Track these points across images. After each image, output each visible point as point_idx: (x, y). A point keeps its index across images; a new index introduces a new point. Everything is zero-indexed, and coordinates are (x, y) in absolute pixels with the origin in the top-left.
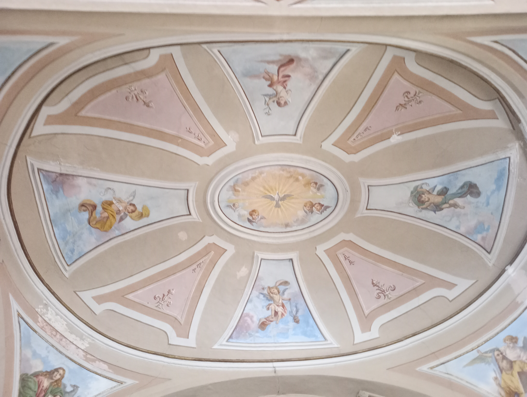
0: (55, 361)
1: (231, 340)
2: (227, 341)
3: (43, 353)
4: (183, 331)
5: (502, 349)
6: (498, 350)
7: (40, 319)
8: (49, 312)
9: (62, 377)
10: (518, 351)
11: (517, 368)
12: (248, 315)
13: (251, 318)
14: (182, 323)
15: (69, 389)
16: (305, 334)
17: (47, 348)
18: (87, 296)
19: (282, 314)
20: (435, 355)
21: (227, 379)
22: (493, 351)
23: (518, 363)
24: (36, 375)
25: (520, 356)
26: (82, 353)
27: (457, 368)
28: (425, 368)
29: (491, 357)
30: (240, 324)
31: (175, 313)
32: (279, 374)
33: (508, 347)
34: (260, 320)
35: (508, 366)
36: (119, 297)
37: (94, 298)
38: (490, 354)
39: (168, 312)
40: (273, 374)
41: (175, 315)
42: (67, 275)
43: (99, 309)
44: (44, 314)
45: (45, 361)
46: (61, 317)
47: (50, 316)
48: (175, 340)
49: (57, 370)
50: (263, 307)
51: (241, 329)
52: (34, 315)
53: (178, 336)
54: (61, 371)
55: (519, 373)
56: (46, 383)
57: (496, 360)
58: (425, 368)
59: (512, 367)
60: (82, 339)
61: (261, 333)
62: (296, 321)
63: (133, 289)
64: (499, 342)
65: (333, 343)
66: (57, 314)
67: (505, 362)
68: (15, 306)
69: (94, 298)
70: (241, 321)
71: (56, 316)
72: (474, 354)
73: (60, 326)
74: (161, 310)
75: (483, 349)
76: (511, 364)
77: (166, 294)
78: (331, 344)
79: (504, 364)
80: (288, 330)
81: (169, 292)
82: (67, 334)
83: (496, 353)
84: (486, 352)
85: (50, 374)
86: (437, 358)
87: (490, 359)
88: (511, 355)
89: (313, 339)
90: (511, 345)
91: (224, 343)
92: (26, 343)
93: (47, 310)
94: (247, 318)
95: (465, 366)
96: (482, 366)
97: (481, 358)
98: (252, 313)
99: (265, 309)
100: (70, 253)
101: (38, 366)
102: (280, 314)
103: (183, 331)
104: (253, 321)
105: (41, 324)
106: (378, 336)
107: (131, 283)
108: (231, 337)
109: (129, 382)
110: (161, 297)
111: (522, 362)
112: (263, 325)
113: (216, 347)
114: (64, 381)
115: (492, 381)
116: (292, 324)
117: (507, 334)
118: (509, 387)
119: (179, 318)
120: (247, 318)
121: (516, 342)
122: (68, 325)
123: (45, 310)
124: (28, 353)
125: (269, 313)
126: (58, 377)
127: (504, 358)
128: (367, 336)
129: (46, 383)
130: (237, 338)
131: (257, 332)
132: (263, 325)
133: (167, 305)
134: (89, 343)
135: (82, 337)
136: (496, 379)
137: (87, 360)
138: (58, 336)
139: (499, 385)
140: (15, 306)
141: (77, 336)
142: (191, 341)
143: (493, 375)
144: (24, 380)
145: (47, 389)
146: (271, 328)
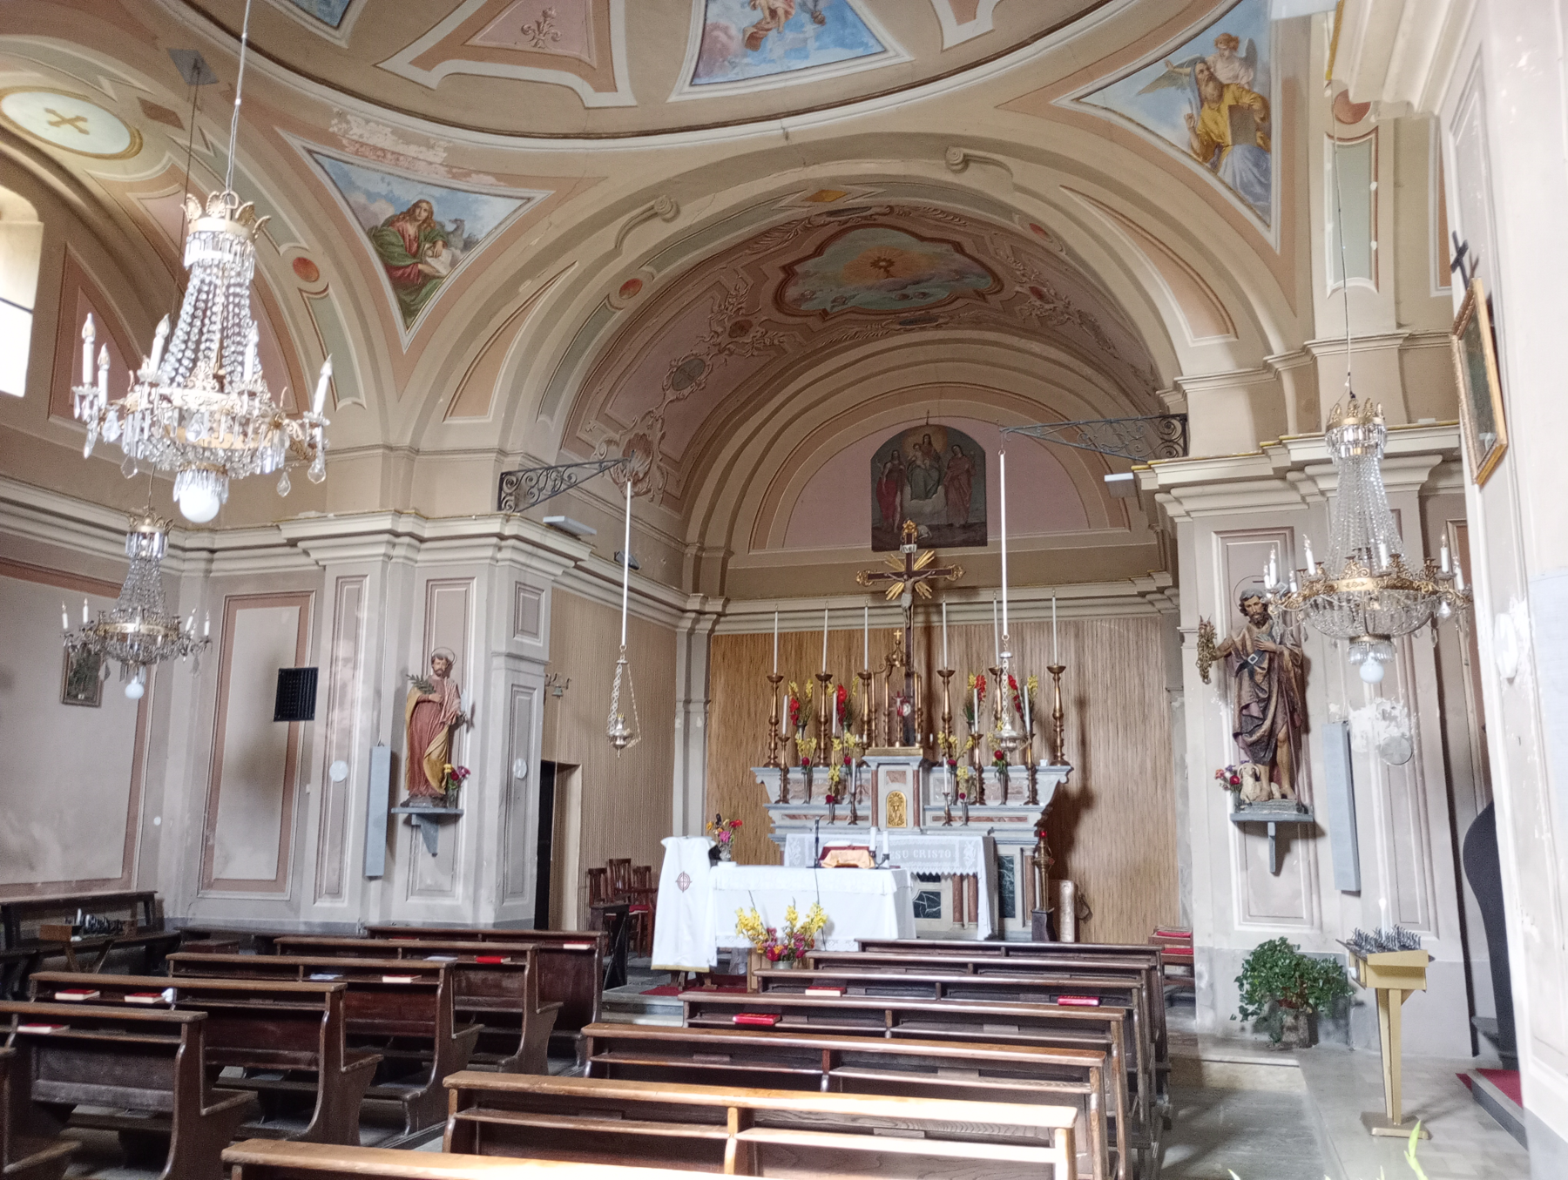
0: (409, 196)
1: (697, 81)
2: (691, 85)
3: (382, 189)
4: (603, 79)
5: (1210, 59)
6: (1203, 61)
7: (345, 142)
8: (353, 124)
9: (431, 213)
10: (1237, 64)
11: (1229, 99)
12: (716, 27)
13: (726, 30)
14: (595, 65)
15: (450, 227)
16: (841, 43)
17: (383, 180)
18: (401, 63)
19: (787, 13)
20: (1087, 72)
21: (703, 163)
22: (1193, 63)
23: (1232, 88)
24: (390, 222)
25: (1236, 77)
26: (443, 170)
27: (1124, 98)
28: (1064, 101)
29: (1188, 75)
30: (706, 47)
31: (574, 51)
32: (795, 141)
33: (1222, 56)
34: (744, 31)
35: (1216, 93)
36: (457, 45)
37: (415, 63)
38: (1188, 70)
39: (559, 51)
40: (783, 143)
41: (574, 52)
42: (343, 44)
43: (433, 78)
44: (346, 132)
45: (390, 199)
46: (378, 123)
47: (356, 131)
48: (594, 99)
49: (416, 205)
50: (742, 6)
51: (710, 57)
52: (333, 140)
53: (598, 89)
54: (424, 205)
55: (1231, 108)
56: (411, 229)
57: (1197, 81)
58: (1064, 101)
59: (1221, 96)
60: (430, 147)
61: (751, 58)
62: (818, 20)
63: (475, 24)
64: (1205, 47)
65: (899, 55)
66: (368, 121)
67: (1211, 85)
68: (296, 143)
69: (415, 63)
70: (707, 41)
71: (368, 126)
72: (1160, 69)
73: (385, 141)
74: (547, 51)
75: (1180, 57)
76: (1221, 88)
77: (541, 20)
78: (897, 55)
79: (1209, 90)
80: (805, 40)
81: (545, 14)
82: (401, 148)
83: (1199, 67)
84: (1181, 66)
85: (410, 213)
86: (1091, 77)
87: (1186, 80)
88: (1224, 73)
89: (860, 51)
90: (1227, 53)
91: (687, 88)
92: (345, 185)
93: (348, 122)
94: (716, 33)
95: (1140, 93)
96: (1172, 91)
97: (1170, 78)
98: (723, 22)
99: (748, 9)
100: (324, 8)
101: (385, 211)
102: (781, 12)
103: (603, 79)
104: (730, 37)
105: (352, 149)
106: (989, 27)
107: (310, 819)
108: (695, 75)
109: (539, 195)
110: (535, 27)
111: (1240, 87)
112: (753, 41)
113: (673, 98)
114: (437, 217)
115: (1182, 122)
116: (810, 28)
117: (1223, 31)
118: (1208, 134)
119: (585, 57)
120: (716, 33)
121: (1235, 48)
122: (395, 132)
123: (344, 126)
124: (359, 198)
125: (757, 15)
126: (424, 215)
127: (1212, 77)
128: (969, 30)
129: (411, 229)
130: (709, 73)
131: (745, 56)
132: (753, 41)
133: (554, 40)
134: (446, 149)
135: (428, 144)
136: (1190, 117)
137: (454, 176)
138: (389, 156)
139: (1193, 129)
140: (296, 143)
141: (419, 145)
142: (624, 95)
143: (1187, 110)
144: (375, 235)
145: (417, 238)
146: (771, 42)
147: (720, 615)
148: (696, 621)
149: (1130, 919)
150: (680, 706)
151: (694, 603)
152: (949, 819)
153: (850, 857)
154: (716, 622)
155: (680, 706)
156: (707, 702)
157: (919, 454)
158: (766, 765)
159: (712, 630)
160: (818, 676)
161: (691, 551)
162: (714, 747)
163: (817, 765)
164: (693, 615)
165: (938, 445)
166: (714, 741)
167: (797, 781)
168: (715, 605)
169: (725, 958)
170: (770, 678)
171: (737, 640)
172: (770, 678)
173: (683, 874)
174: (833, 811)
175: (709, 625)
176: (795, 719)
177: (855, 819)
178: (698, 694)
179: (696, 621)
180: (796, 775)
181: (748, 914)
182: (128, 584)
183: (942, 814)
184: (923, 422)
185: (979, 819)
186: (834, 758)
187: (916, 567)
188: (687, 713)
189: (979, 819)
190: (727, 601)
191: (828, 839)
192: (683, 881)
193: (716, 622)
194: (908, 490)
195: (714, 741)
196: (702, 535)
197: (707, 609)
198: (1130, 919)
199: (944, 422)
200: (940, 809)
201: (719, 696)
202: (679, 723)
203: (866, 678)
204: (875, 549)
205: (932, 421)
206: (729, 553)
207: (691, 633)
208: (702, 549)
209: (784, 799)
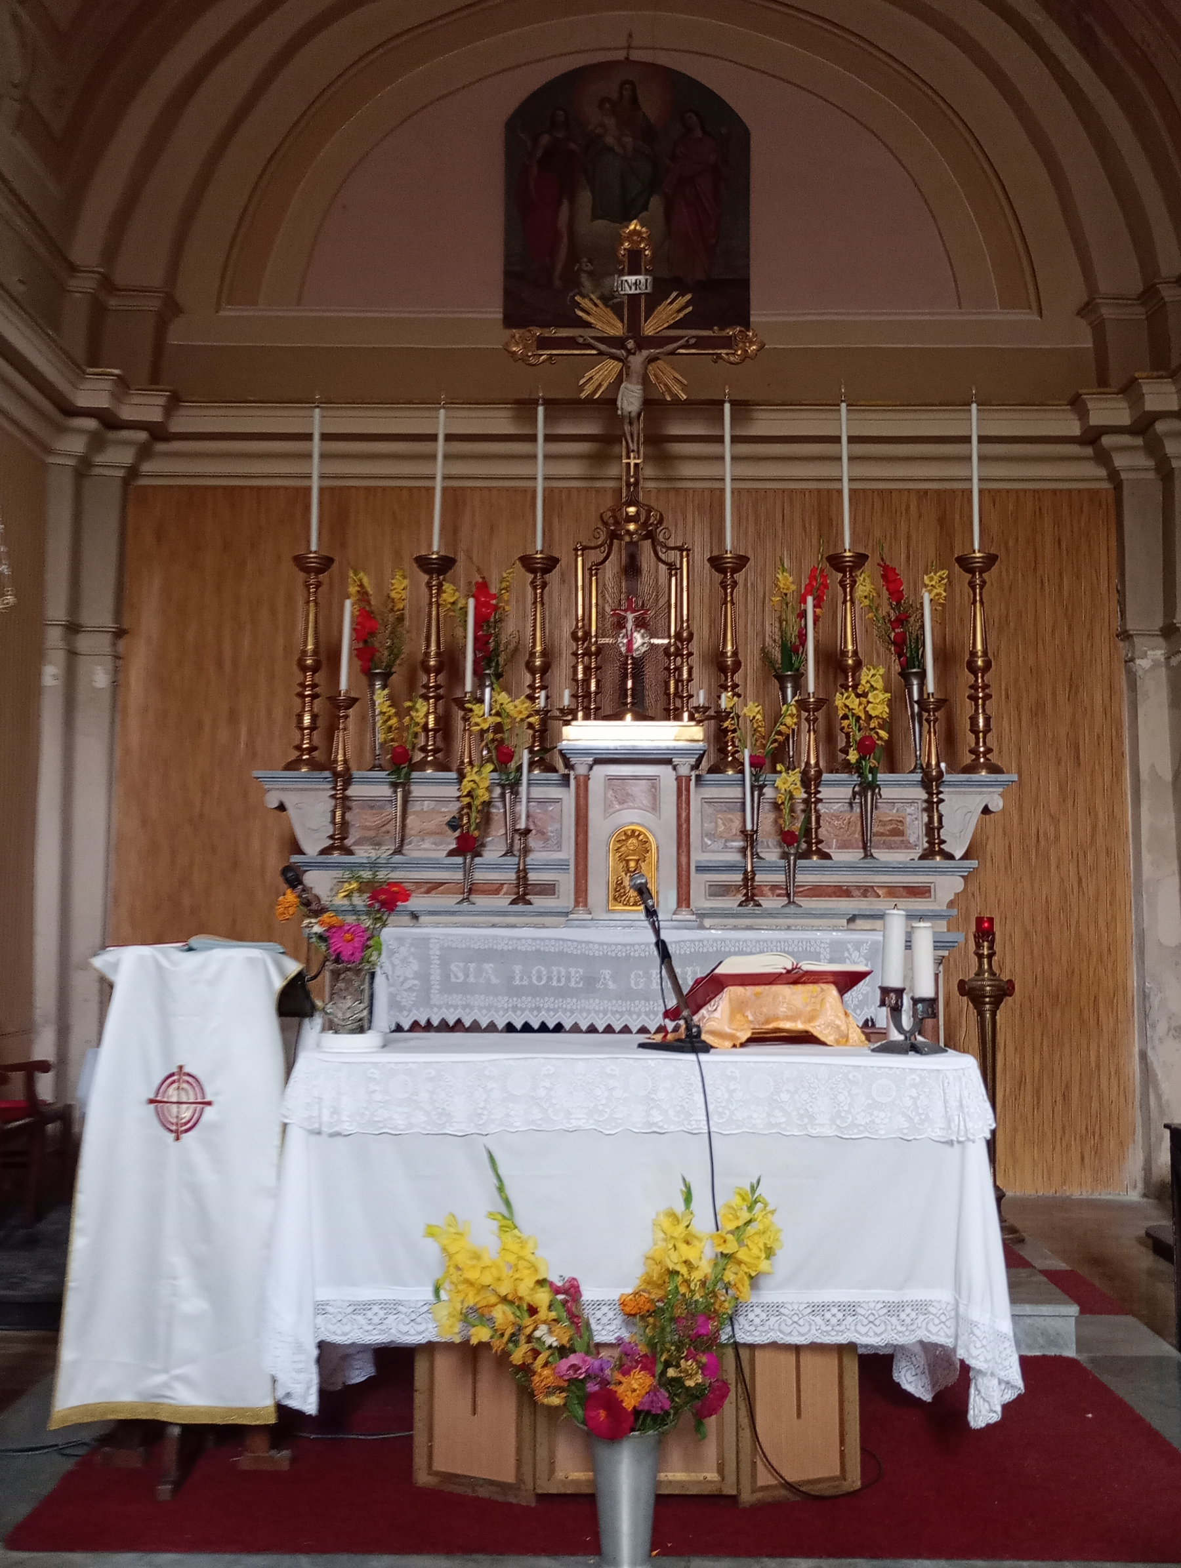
147: (158, 433)
148: (97, 443)
149: (1037, 1093)
150: (54, 636)
151: (93, 394)
152: (750, 892)
153: (789, 1006)
154: (144, 452)
155: (54, 636)
156: (120, 633)
157: (610, 122)
158: (292, 766)
159: (133, 472)
160: (423, 562)
161: (83, 284)
162: (135, 739)
163: (422, 766)
164: (91, 424)
165: (651, 106)
166: (134, 722)
167: (372, 804)
168: (146, 408)
169: (374, 1389)
170: (300, 561)
171: (193, 498)
172: (300, 561)
173: (178, 1076)
174: (468, 870)
175: (126, 457)
176: (365, 654)
177: (523, 891)
178: (99, 612)
179: (97, 443)
180: (371, 788)
181: (484, 1235)
182: (588, 1358)
183: (738, 878)
184: (620, 55)
185: (817, 891)
186: (463, 746)
187: (649, 329)
188: (72, 654)
189: (817, 891)
190: (174, 402)
191: (699, 943)
192: (178, 1103)
193: (144, 452)
194: (585, 198)
195: (134, 722)
196: (110, 253)
197: (127, 413)
198: (1037, 1093)
199: (663, 59)
200: (730, 868)
201: (149, 621)
202: (51, 675)
203: (541, 568)
204: (510, 321)
205: (636, 55)
206: (171, 308)
207: (83, 468)
208: (107, 284)
209: (339, 843)
